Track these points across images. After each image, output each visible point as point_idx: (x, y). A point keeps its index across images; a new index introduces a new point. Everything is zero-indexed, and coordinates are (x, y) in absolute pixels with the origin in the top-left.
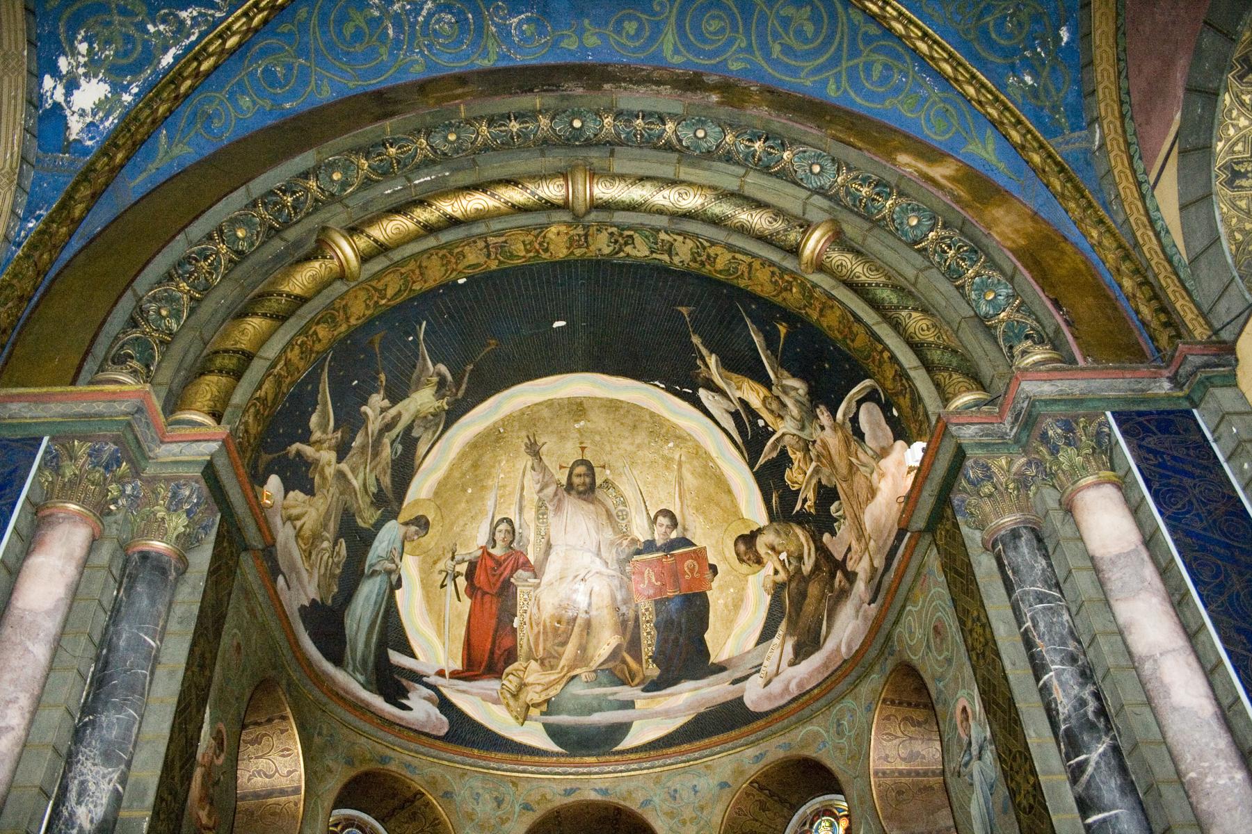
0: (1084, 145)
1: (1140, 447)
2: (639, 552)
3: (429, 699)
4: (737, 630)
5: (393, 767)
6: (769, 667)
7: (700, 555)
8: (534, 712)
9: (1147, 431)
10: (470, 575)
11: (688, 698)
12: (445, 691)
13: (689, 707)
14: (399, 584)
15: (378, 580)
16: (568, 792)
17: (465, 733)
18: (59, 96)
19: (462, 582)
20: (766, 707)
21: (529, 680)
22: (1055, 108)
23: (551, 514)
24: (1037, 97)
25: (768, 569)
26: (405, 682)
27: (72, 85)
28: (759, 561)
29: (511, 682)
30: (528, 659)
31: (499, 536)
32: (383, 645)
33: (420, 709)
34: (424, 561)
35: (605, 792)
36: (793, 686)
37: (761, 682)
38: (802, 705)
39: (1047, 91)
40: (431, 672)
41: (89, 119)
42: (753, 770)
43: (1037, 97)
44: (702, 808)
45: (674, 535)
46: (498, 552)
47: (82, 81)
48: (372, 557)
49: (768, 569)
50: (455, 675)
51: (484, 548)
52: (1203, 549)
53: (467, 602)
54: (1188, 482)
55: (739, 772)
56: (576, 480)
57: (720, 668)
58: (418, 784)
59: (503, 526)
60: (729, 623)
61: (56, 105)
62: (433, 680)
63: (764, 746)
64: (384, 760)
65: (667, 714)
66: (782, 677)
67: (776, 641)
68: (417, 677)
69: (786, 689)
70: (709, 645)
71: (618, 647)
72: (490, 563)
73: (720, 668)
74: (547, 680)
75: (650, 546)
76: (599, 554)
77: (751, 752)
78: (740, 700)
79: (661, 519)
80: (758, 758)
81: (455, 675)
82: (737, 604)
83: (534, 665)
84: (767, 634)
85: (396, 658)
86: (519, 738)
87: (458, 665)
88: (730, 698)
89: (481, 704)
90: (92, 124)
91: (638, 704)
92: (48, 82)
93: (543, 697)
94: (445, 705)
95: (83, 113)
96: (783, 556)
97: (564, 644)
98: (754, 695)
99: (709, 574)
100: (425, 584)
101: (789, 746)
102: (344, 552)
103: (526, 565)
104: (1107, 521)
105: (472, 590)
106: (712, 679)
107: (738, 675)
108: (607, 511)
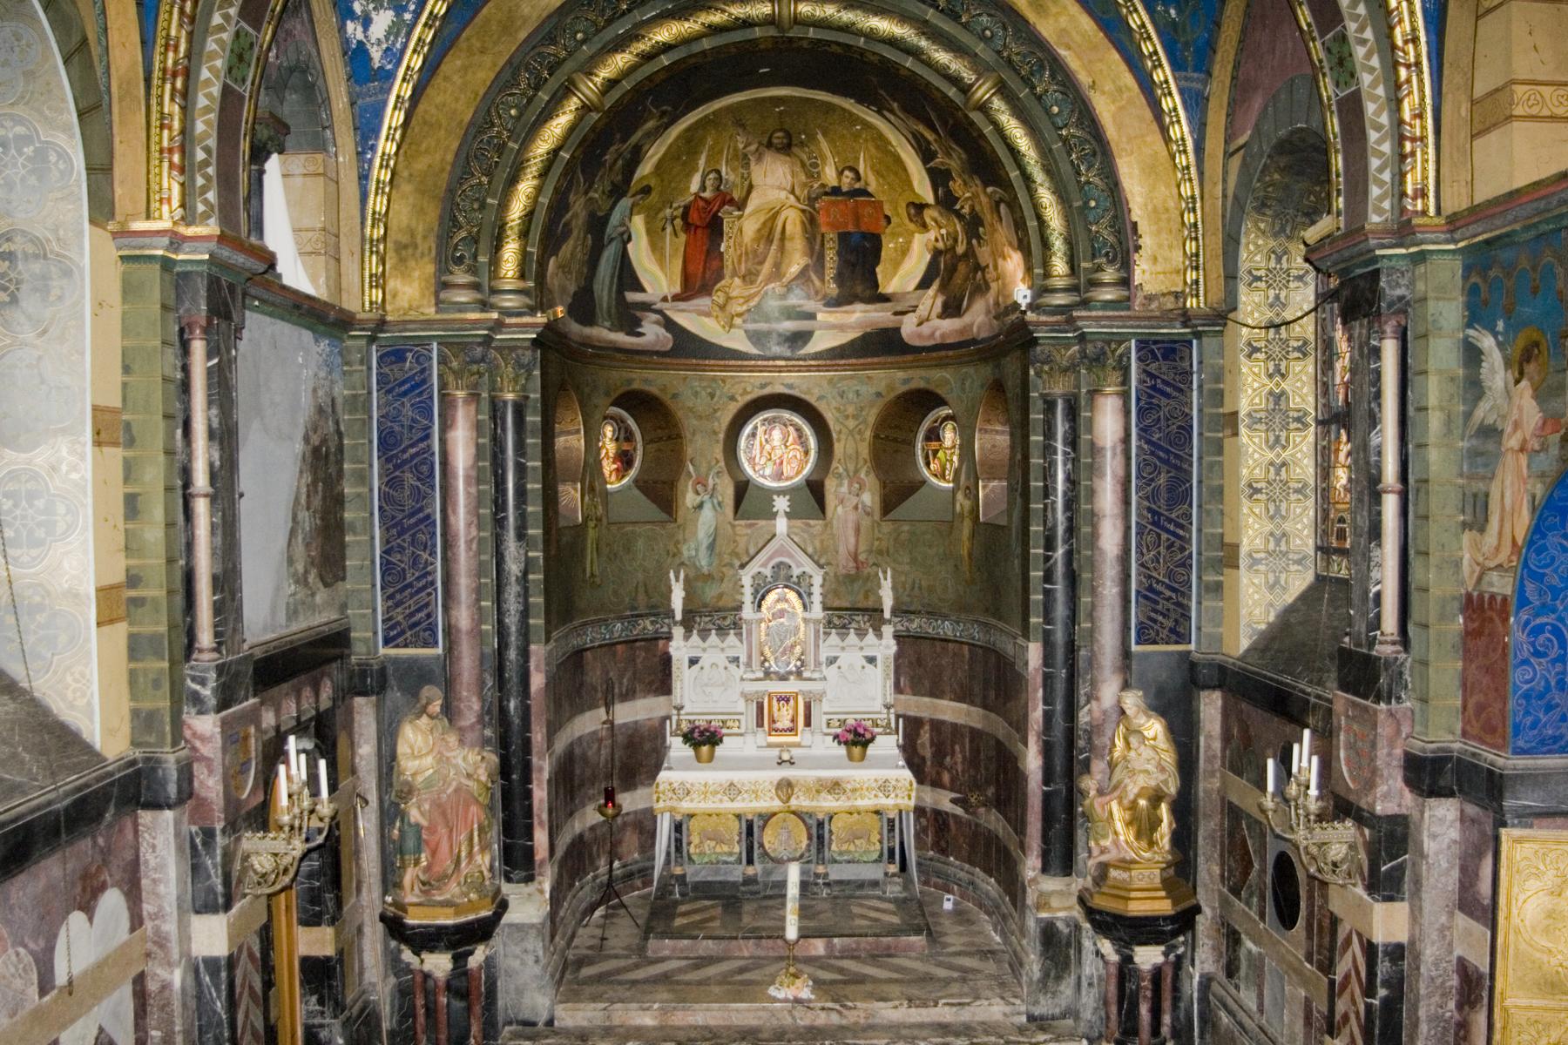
0: (1199, 86)
1: (1145, 371)
2: (826, 194)
3: (657, 323)
4: (901, 272)
5: (636, 386)
6: (923, 310)
7: (878, 206)
8: (738, 321)
9: (1155, 358)
10: (685, 216)
11: (859, 318)
12: (668, 313)
13: (859, 325)
14: (630, 239)
15: (614, 244)
16: (763, 386)
17: (688, 347)
18: (360, 36)
19: (678, 222)
20: (917, 343)
21: (734, 294)
22: (1186, 44)
23: (752, 164)
24: (1175, 30)
25: (932, 235)
26: (638, 314)
27: (366, 22)
28: (924, 226)
29: (719, 297)
30: (732, 277)
31: (708, 183)
32: (620, 292)
33: (652, 333)
34: (647, 217)
35: (791, 386)
36: (938, 334)
37: (915, 321)
38: (940, 352)
39: (1184, 30)
40: (657, 299)
41: (384, 46)
42: (903, 389)
43: (1175, 30)
44: (862, 409)
45: (857, 186)
46: (707, 194)
47: (373, 15)
48: (609, 230)
49: (932, 235)
50: (676, 298)
51: (696, 195)
52: (1152, 453)
53: (683, 237)
54: (1164, 401)
55: (890, 387)
56: (775, 141)
57: (885, 299)
58: (654, 390)
59: (712, 176)
60: (897, 264)
61: (360, 42)
62: (658, 306)
63: (911, 373)
64: (630, 381)
65: (841, 328)
66: (931, 323)
67: (931, 292)
68: (647, 307)
69: (933, 334)
70: (879, 277)
71: (807, 266)
72: (701, 204)
73: (885, 299)
74: (746, 294)
75: (836, 191)
76: (792, 192)
77: (901, 374)
78: (897, 330)
79: (847, 173)
80: (906, 381)
81: (676, 298)
82: (904, 251)
83: (737, 281)
84: (924, 284)
85: (632, 297)
86: (726, 344)
87: (677, 289)
88: (891, 325)
89: (697, 320)
90: (388, 49)
91: (820, 316)
92: (350, 26)
93: (745, 307)
94: (669, 325)
95: (379, 42)
96: (943, 231)
97: (761, 263)
98: (909, 328)
99: (883, 222)
100: (649, 232)
101: (928, 381)
102: (590, 242)
103: (731, 202)
104: (1108, 422)
105: (687, 226)
106: (878, 306)
107: (899, 308)
108: (802, 162)
